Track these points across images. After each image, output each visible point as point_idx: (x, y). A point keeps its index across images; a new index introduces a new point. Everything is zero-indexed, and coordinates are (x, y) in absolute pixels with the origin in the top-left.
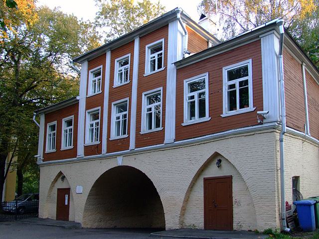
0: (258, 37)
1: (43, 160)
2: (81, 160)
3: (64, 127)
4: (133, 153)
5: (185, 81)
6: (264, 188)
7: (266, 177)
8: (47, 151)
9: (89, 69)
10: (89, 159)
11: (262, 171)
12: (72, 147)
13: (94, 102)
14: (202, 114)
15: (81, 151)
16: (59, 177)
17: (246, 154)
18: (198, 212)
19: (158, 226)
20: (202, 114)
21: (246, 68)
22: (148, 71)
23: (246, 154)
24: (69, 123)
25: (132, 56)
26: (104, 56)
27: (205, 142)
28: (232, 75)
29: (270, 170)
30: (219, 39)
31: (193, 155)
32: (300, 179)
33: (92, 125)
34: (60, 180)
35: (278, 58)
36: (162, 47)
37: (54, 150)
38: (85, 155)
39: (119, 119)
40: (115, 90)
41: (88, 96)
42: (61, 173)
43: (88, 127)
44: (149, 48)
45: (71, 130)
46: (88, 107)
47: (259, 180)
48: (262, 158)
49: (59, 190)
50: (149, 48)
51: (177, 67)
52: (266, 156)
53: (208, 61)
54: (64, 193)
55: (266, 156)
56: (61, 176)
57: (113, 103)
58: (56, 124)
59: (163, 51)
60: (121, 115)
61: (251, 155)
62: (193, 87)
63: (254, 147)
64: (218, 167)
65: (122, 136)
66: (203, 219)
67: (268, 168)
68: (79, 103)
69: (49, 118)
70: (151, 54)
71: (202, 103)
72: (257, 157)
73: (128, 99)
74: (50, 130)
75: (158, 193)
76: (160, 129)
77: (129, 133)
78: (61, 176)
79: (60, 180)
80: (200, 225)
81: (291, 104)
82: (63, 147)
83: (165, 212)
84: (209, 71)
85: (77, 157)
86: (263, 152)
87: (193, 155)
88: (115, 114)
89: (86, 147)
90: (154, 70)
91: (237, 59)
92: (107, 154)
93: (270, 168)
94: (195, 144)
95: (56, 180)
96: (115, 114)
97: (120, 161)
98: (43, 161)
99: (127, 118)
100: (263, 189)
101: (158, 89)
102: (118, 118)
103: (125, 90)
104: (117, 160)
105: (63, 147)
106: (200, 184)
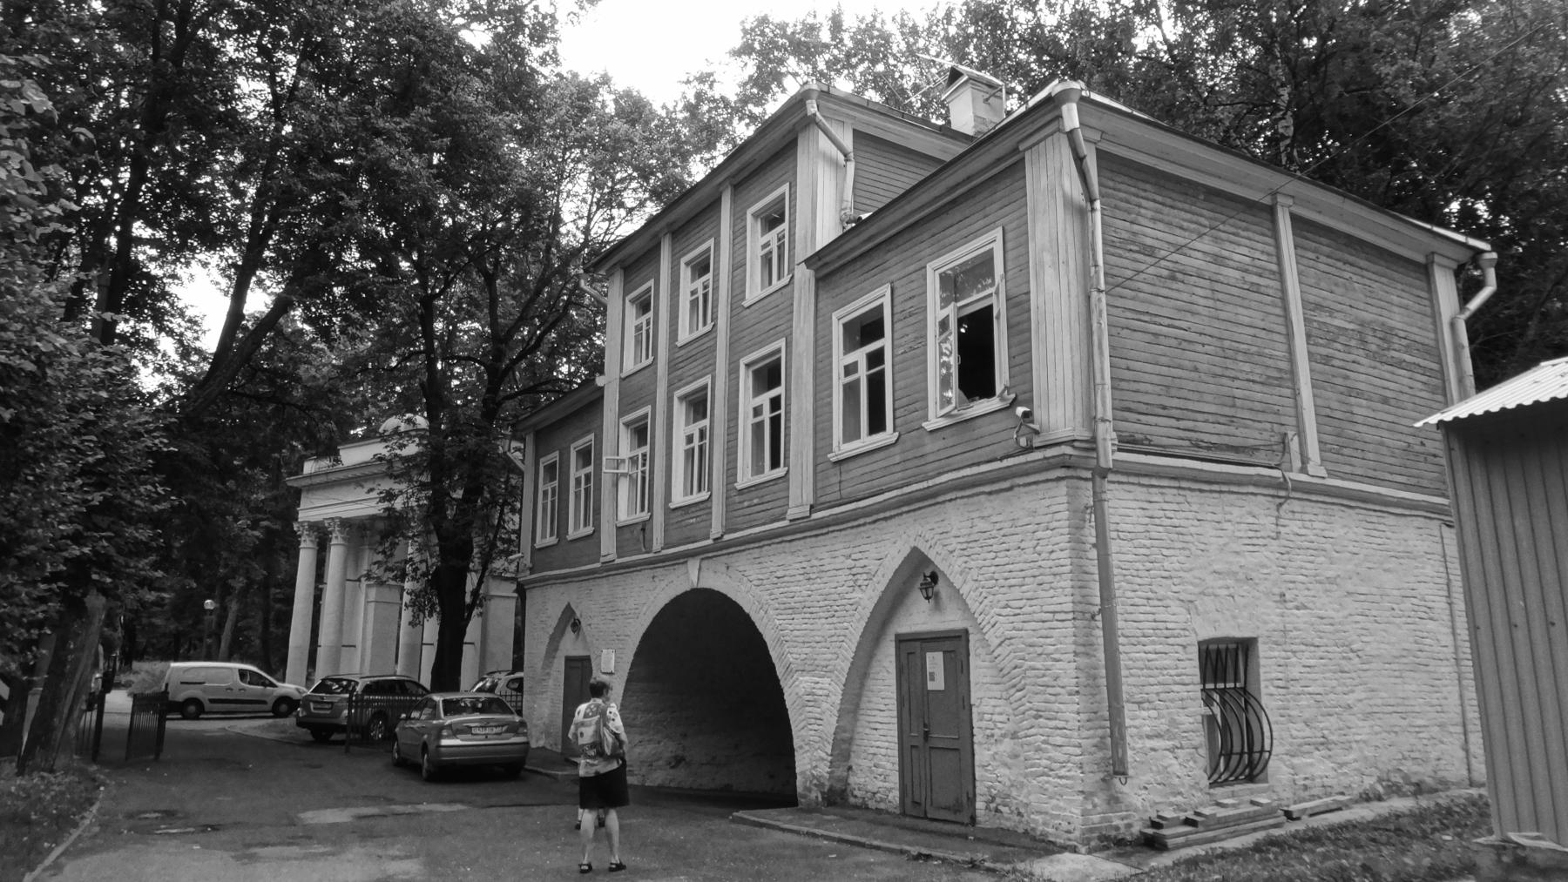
0: (1015, 150)
1: (531, 569)
3: (575, 472)
5: (834, 317)
6: (1045, 679)
7: (1048, 641)
8: (539, 543)
10: (628, 567)
11: (1037, 616)
14: (877, 425)
15: (608, 546)
17: (992, 555)
18: (883, 751)
20: (877, 425)
23: (992, 555)
25: (717, 244)
26: (715, 204)
28: (953, 285)
29: (1058, 616)
33: (690, 439)
34: (569, 634)
36: (782, 215)
39: (856, 371)
40: (683, 352)
41: (623, 376)
42: (568, 612)
43: (745, 422)
44: (756, 216)
45: (588, 477)
47: (1031, 649)
48: (1036, 572)
49: (569, 660)
51: (816, 271)
58: (887, 301)
59: (785, 226)
60: (695, 429)
63: (1013, 530)
64: (928, 598)
65: (769, 474)
66: (895, 778)
67: (1052, 608)
68: (602, 397)
70: (763, 235)
72: (1022, 566)
73: (782, 343)
75: (778, 681)
76: (780, 472)
77: (650, 510)
80: (891, 796)
82: (572, 534)
83: (797, 742)
84: (893, 277)
86: (1038, 548)
90: (770, 283)
91: (964, 232)
93: (1058, 608)
94: (861, 521)
100: (1040, 681)
101: (877, 292)
102: (757, 411)
103: (702, 349)
106: (888, 651)
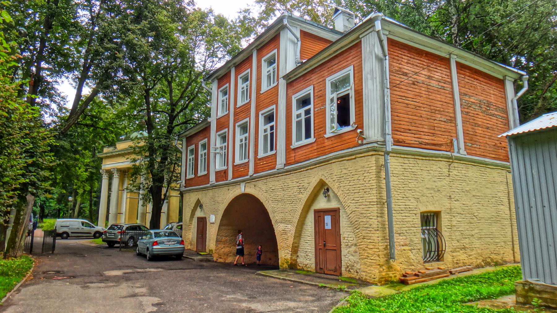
0: (358, 38)
2: (214, 187)
3: (201, 152)
4: (252, 179)
5: (293, 97)
9: (219, 87)
12: (206, 172)
13: (222, 124)
14: (308, 136)
15: (212, 178)
16: (197, 207)
19: (272, 262)
20: (308, 136)
21: (348, 76)
22: (265, 88)
23: (349, 182)
24: (204, 146)
27: (312, 167)
28: (336, 86)
30: (342, 31)
31: (301, 182)
32: (442, 214)
33: (241, 141)
34: (199, 209)
35: (381, 61)
37: (193, 176)
38: (217, 181)
41: (218, 118)
44: (265, 61)
45: (205, 154)
46: (218, 129)
47: (362, 215)
49: (198, 218)
50: (265, 61)
51: (287, 81)
52: (369, 185)
53: (297, 81)
54: (202, 222)
55: (369, 185)
56: (199, 204)
57: (260, 113)
58: (312, 92)
61: (353, 184)
62: (305, 102)
63: (356, 173)
65: (270, 153)
69: (189, 140)
71: (308, 121)
72: (358, 186)
74: (202, 149)
75: (272, 226)
76: (274, 152)
78: (199, 204)
79: (199, 209)
81: (415, 116)
82: (200, 174)
85: (210, 183)
87: (301, 182)
88: (239, 136)
89: (217, 173)
92: (232, 181)
95: (313, 198)
96: (238, 137)
97: (242, 189)
98: (185, 187)
99: (274, 131)
101: (204, 140)
104: (240, 188)
105: (200, 174)
